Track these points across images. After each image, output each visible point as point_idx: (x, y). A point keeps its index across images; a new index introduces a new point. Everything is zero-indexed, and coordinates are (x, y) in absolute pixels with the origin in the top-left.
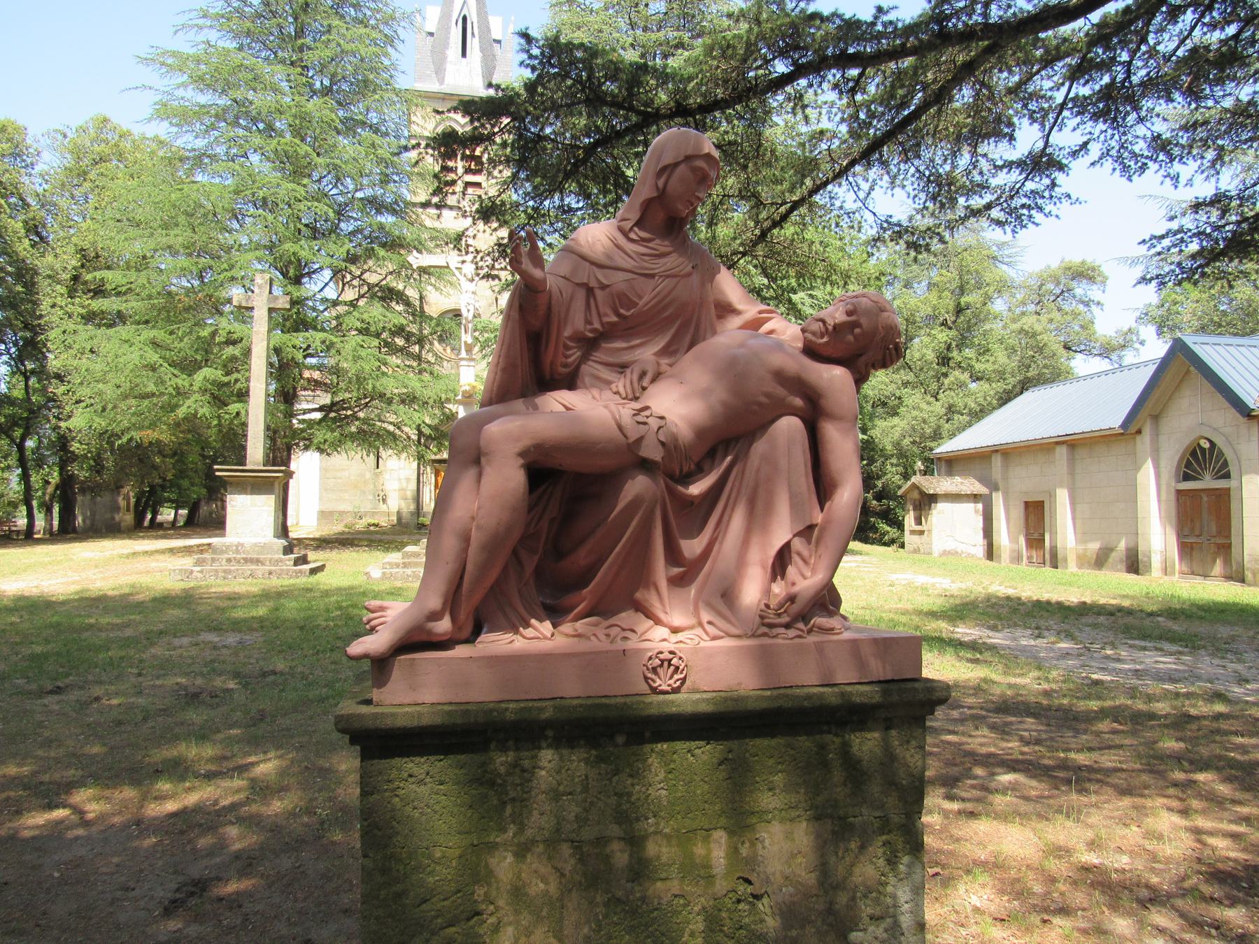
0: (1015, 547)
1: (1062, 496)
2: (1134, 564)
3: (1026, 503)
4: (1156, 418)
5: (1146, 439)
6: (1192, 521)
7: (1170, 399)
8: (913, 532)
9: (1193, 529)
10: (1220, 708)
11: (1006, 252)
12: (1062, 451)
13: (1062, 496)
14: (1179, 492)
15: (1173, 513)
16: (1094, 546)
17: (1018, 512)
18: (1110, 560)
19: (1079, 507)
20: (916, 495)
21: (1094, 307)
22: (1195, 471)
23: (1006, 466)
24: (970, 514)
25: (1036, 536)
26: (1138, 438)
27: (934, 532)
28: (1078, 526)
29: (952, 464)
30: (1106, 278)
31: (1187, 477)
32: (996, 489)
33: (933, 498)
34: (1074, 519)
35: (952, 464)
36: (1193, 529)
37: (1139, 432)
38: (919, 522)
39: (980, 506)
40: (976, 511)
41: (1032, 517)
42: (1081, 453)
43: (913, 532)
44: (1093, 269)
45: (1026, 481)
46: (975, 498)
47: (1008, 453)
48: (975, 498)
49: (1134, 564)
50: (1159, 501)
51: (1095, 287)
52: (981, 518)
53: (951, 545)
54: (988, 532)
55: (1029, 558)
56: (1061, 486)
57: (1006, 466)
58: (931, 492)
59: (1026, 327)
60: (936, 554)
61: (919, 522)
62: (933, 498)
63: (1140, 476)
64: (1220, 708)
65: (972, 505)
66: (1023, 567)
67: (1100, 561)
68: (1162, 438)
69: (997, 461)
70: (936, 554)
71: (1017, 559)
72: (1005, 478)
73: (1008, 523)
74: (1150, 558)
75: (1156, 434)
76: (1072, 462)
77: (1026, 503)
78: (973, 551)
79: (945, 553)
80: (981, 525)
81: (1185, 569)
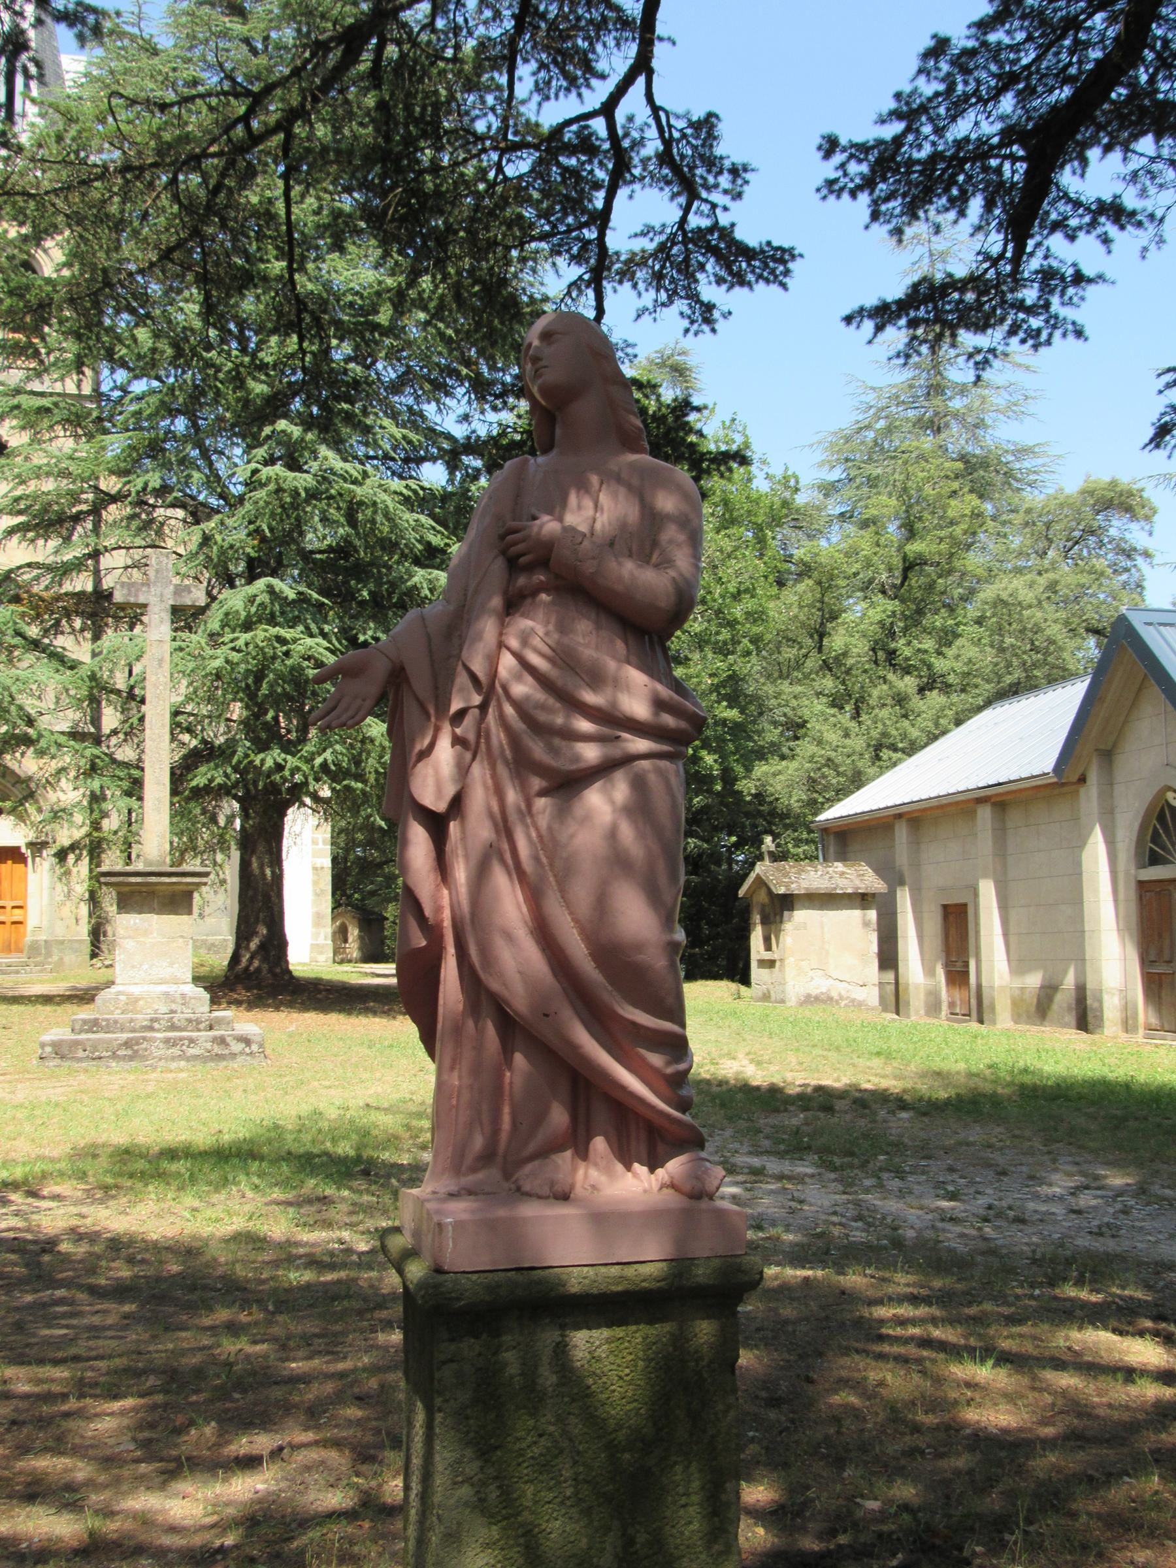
0: (930, 982)
1: (988, 892)
2: (1084, 1018)
3: (945, 907)
4: (1108, 756)
5: (1091, 795)
6: (1160, 936)
7: (1125, 722)
8: (763, 963)
9: (1160, 952)
10: (973, 1311)
11: (1026, 464)
12: (985, 814)
13: (988, 892)
14: (1141, 884)
15: (1134, 919)
16: (1034, 980)
17: (934, 923)
18: (1055, 1007)
19: (1013, 915)
20: (762, 897)
21: (1140, 561)
22: (1164, 848)
23: (915, 844)
24: (855, 930)
25: (959, 967)
26: (1082, 790)
27: (790, 961)
28: (1012, 946)
29: (845, 840)
30: (1154, 511)
31: (1155, 860)
32: (902, 883)
33: (787, 902)
34: (1006, 935)
35: (845, 840)
36: (1160, 952)
37: (1082, 780)
38: (768, 948)
39: (872, 914)
40: (866, 924)
41: (953, 931)
42: (1015, 817)
43: (763, 963)
44: (1130, 494)
45: (941, 862)
46: (863, 900)
47: (917, 818)
48: (863, 900)
49: (1084, 1018)
50: (1116, 901)
51: (1134, 526)
52: (874, 937)
53: (819, 985)
54: (888, 958)
55: (952, 1005)
56: (985, 876)
57: (915, 844)
58: (782, 890)
59: (1004, 595)
60: (792, 1001)
61: (768, 948)
62: (787, 902)
63: (1086, 855)
64: (973, 1311)
65: (857, 913)
66: (942, 1022)
67: (1041, 1007)
68: (1119, 789)
69: (902, 833)
70: (792, 1001)
71: (933, 1008)
72: (916, 865)
73: (920, 937)
74: (1100, 1002)
75: (1109, 782)
76: (1001, 834)
77: (945, 907)
78: (859, 994)
79: (810, 1000)
80: (874, 948)
81: (1154, 1021)
